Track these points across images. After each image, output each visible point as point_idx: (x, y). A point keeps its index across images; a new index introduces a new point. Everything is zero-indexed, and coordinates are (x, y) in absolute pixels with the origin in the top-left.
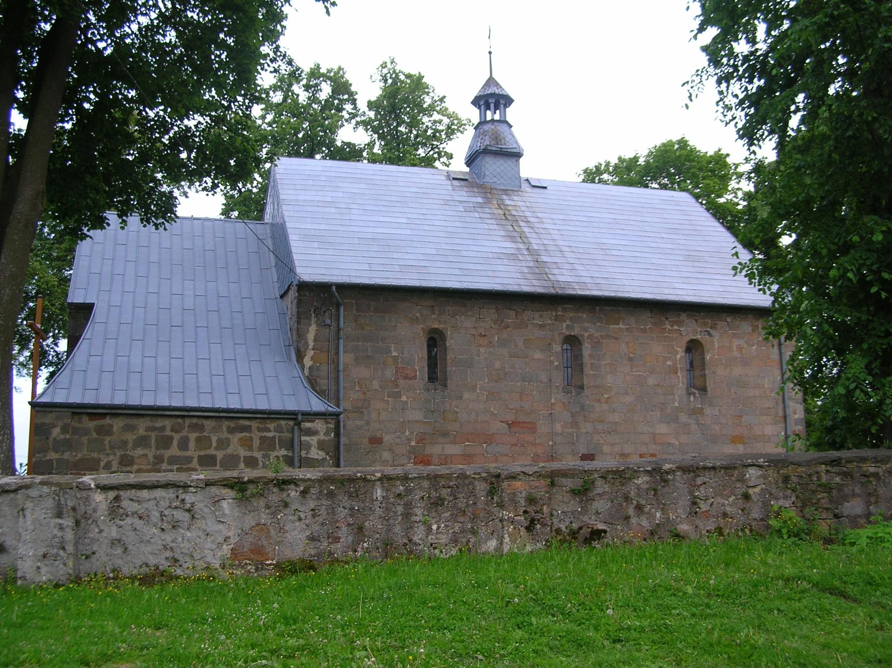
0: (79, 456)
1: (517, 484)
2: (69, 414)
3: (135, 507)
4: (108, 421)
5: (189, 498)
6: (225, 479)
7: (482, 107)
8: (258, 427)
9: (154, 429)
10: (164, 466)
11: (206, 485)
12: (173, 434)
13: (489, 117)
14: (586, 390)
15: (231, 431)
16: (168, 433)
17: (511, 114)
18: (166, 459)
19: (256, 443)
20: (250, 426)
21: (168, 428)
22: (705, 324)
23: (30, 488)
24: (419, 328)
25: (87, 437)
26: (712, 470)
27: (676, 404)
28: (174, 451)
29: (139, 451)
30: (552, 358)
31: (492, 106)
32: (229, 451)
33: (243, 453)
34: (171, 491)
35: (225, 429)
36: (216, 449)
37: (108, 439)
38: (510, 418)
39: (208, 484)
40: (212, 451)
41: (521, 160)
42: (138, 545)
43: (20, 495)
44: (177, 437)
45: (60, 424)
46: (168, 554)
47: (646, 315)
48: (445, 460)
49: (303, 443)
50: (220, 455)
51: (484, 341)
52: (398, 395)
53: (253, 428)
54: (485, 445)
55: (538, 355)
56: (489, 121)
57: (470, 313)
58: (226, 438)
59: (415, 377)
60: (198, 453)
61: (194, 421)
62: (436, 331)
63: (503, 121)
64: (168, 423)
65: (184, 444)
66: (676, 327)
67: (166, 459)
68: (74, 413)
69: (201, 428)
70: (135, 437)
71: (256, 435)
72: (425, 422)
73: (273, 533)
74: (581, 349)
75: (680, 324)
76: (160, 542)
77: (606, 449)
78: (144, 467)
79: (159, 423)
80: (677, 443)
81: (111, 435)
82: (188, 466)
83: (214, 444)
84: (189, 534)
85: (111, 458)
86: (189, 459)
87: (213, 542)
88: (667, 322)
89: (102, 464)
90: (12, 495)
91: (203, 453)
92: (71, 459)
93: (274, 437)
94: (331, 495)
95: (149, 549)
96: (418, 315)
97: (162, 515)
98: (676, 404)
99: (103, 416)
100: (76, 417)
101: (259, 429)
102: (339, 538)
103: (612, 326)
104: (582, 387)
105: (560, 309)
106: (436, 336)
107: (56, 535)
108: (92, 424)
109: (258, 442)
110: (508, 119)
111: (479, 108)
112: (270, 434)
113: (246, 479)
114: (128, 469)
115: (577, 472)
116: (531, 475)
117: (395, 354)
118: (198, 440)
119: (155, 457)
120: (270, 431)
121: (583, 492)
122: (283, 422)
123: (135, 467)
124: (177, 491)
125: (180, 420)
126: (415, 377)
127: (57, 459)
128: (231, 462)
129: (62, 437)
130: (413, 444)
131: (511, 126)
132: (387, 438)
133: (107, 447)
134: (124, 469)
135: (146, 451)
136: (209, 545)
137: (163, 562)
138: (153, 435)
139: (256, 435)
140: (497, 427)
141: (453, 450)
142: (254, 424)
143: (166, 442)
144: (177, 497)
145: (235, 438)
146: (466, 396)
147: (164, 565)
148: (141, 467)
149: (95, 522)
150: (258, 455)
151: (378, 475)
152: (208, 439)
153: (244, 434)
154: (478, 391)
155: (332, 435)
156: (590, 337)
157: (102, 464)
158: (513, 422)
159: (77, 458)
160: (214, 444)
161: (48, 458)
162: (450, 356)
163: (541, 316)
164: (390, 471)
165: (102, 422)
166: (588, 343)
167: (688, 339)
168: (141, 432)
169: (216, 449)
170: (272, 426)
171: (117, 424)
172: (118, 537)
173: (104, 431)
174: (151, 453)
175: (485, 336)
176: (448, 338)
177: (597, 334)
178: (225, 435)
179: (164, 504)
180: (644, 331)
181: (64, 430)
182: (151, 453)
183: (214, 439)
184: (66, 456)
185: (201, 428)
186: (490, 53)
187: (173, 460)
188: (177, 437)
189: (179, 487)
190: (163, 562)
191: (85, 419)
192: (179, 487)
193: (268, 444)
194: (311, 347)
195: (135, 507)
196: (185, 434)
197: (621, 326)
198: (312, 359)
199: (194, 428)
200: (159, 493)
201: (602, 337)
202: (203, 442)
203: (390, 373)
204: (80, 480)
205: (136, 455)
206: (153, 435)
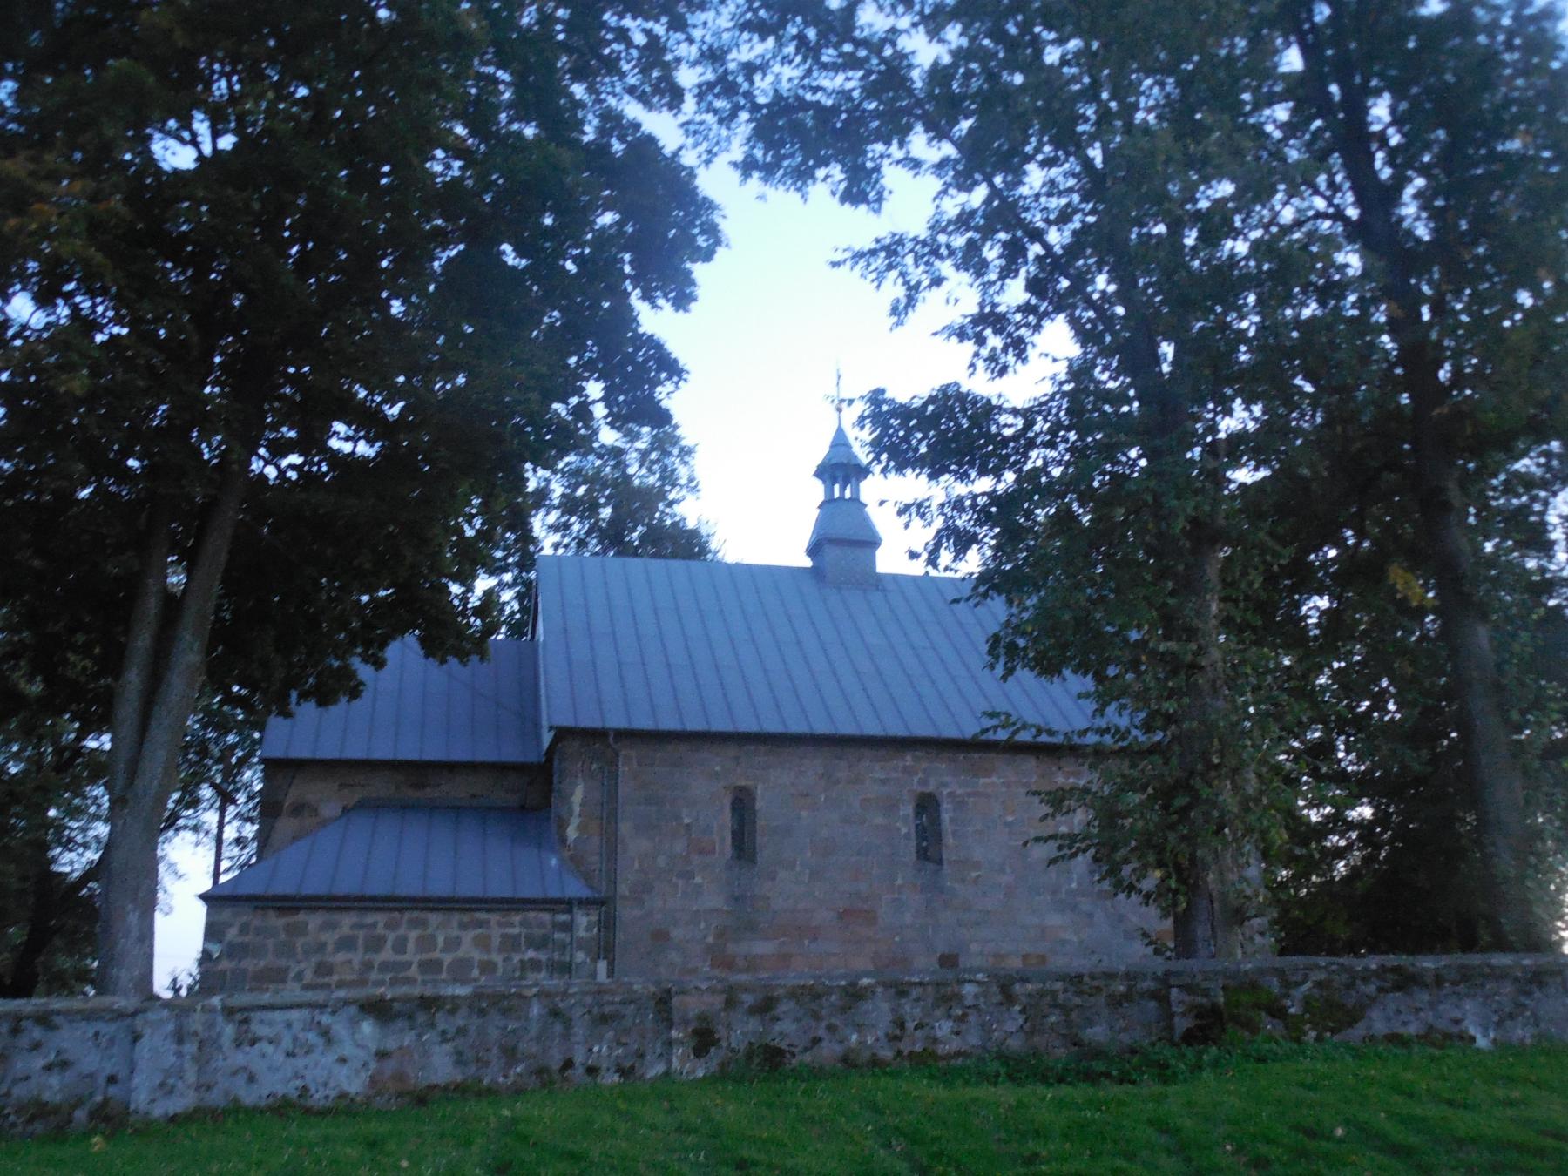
0: (262, 963)
1: (688, 999)
4: (301, 917)
12: (387, 932)
13: (837, 494)
14: (945, 866)
15: (463, 926)
16: (380, 930)
18: (376, 966)
20: (488, 922)
21: (381, 925)
28: (387, 955)
29: (340, 957)
31: (840, 479)
32: (461, 953)
33: (477, 955)
36: (442, 951)
37: (300, 942)
40: (436, 955)
46: (299, 1083)
48: (752, 964)
50: (447, 959)
52: (688, 876)
53: (492, 923)
59: (713, 851)
60: (418, 957)
61: (416, 914)
62: (741, 789)
63: (855, 499)
64: (380, 918)
65: (400, 946)
67: (376, 966)
69: (423, 924)
77: (974, 947)
79: (370, 918)
80: (1075, 939)
85: (303, 966)
86: (408, 965)
88: (1060, 773)
89: (292, 974)
91: (426, 956)
93: (520, 935)
94: (482, 1013)
98: (1074, 885)
101: (500, 924)
103: (982, 780)
104: (940, 862)
105: (909, 758)
112: (516, 931)
117: (687, 821)
118: (420, 940)
121: (765, 1007)
122: (532, 915)
123: (335, 978)
125: (396, 915)
126: (713, 851)
129: (240, 940)
132: (677, 933)
135: (350, 956)
138: (361, 934)
141: (762, 948)
142: (494, 918)
143: (376, 944)
145: (468, 936)
146: (782, 874)
147: (294, 1095)
149: (220, 1048)
150: (497, 958)
152: (433, 937)
153: (480, 931)
154: (798, 869)
155: (596, 930)
157: (292, 974)
161: (219, 968)
162: (760, 823)
169: (442, 951)
170: (517, 918)
171: (314, 921)
173: (295, 931)
174: (357, 958)
176: (759, 798)
177: (959, 791)
178: (455, 932)
179: (297, 1026)
181: (244, 930)
182: (357, 958)
183: (440, 940)
185: (423, 924)
187: (385, 967)
188: (391, 937)
191: (271, 913)
198: (579, 828)
199: (414, 924)
201: (969, 795)
202: (426, 943)
203: (680, 847)
206: (361, 934)
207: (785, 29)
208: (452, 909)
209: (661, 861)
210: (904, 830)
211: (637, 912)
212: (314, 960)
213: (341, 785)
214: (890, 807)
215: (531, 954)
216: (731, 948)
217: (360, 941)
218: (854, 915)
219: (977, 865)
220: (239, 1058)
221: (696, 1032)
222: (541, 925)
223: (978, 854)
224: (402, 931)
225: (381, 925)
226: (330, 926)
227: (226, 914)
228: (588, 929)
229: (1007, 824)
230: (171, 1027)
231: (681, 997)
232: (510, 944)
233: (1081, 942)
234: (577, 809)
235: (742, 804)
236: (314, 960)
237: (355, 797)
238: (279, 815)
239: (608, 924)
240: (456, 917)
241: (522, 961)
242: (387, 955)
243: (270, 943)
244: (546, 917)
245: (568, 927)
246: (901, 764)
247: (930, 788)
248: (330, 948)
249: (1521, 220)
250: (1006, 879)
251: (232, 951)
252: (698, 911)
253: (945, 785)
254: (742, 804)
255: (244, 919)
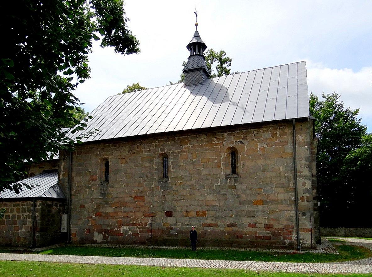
15: (14, 206)
32: (13, 213)
33: (17, 214)
40: (9, 214)
50: (11, 215)
52: (90, 187)
59: (97, 180)
80: (218, 205)
112: (24, 207)
117: (90, 170)
126: (97, 180)
141: (109, 210)
150: (21, 215)
170: (25, 203)
177: (176, 151)
203: (88, 178)
209: (83, 184)
215: (28, 213)
216: (101, 210)
218: (139, 198)
219: (181, 178)
223: (181, 174)
229: (194, 162)
232: (24, 211)
233: (220, 206)
234: (62, 169)
237: (42, 170)
246: (154, 144)
249: (74, 16)
250: (193, 182)
252: (92, 198)
253: (170, 150)
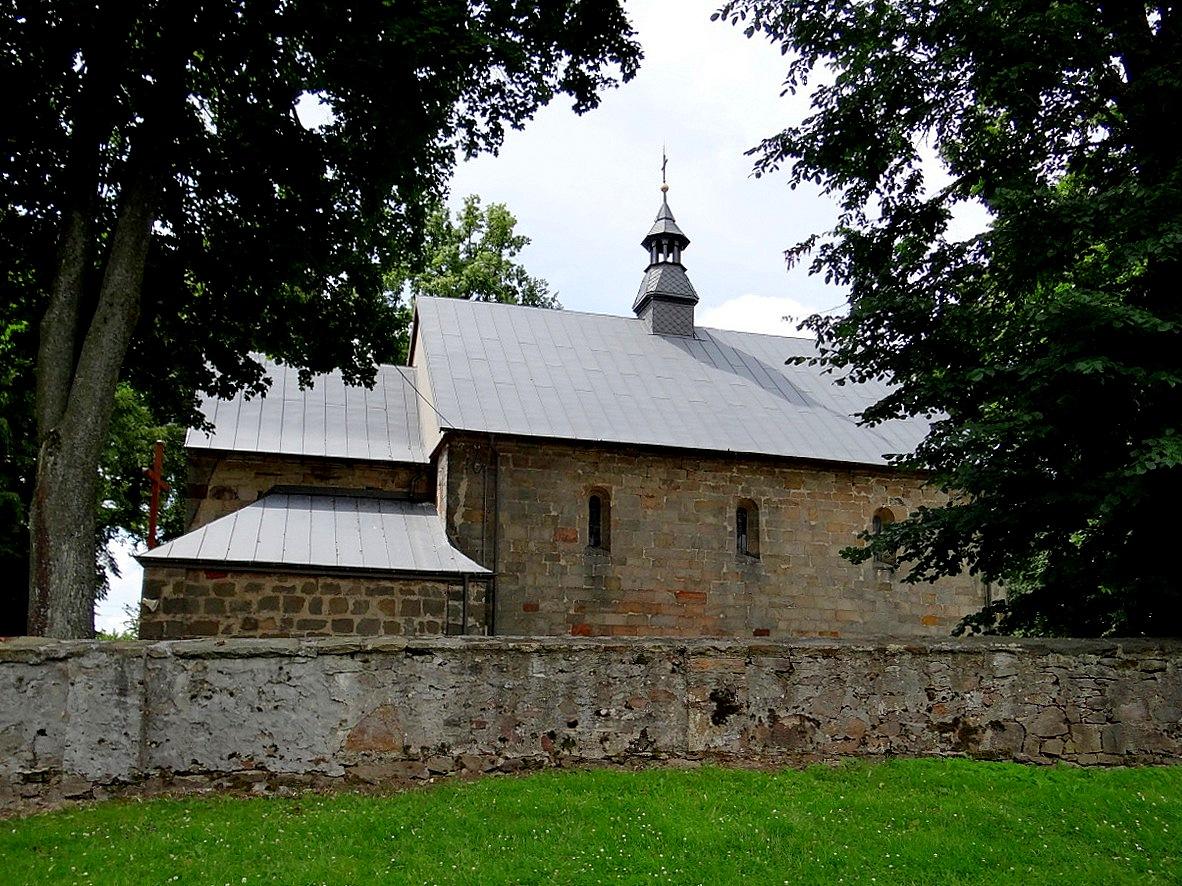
1: (709, 662)
2: (184, 571)
3: (226, 682)
4: (229, 579)
5: (296, 670)
6: (343, 647)
7: (654, 249)
8: (401, 589)
9: (283, 589)
10: (294, 631)
11: (318, 654)
12: (304, 595)
15: (370, 593)
16: (298, 593)
17: (686, 257)
18: (295, 624)
19: (398, 607)
21: (299, 589)
22: (896, 491)
23: (83, 656)
24: (580, 486)
25: (204, 598)
26: (949, 655)
27: (861, 578)
28: (305, 614)
29: (265, 614)
30: (725, 524)
32: (368, 615)
34: (273, 661)
35: (363, 591)
36: (352, 613)
37: (228, 600)
38: (678, 587)
39: (322, 653)
40: (348, 616)
41: (696, 308)
42: (226, 730)
43: (71, 664)
44: (308, 598)
45: (172, 581)
46: (268, 742)
47: (831, 478)
49: (450, 608)
50: (357, 620)
51: (650, 502)
52: (557, 558)
54: (650, 616)
55: (711, 520)
56: (662, 263)
57: (637, 472)
58: (365, 601)
59: (575, 540)
61: (329, 580)
63: (677, 264)
64: (298, 583)
65: (316, 608)
66: (863, 494)
67: (295, 624)
68: (188, 570)
69: (337, 589)
70: (260, 598)
71: (398, 598)
72: (586, 589)
73: (401, 717)
74: (757, 515)
75: (868, 490)
76: (256, 726)
77: (782, 625)
78: (270, 633)
80: (861, 621)
81: (232, 595)
82: (321, 631)
83: (351, 607)
84: (294, 717)
85: (231, 621)
86: (323, 624)
87: (324, 727)
89: (221, 628)
90: (60, 664)
91: (338, 617)
92: (185, 622)
93: (418, 602)
95: (242, 734)
96: (580, 472)
97: (261, 692)
98: (861, 578)
99: (224, 573)
100: (191, 574)
102: (486, 723)
104: (757, 556)
106: (599, 495)
107: (116, 717)
108: (210, 583)
109: (401, 606)
110: (682, 263)
111: (651, 251)
113: (369, 648)
114: (251, 633)
115: (781, 650)
116: (725, 652)
118: (332, 602)
119: (284, 621)
120: (414, 594)
122: (429, 584)
123: (260, 632)
124: (281, 662)
125: (312, 580)
126: (575, 540)
127: (167, 622)
128: (369, 627)
130: (572, 612)
131: (685, 270)
133: (228, 609)
134: (247, 634)
136: (319, 731)
137: (260, 751)
139: (398, 598)
140: (663, 596)
141: (611, 619)
142: (397, 586)
143: (295, 604)
144: (281, 668)
145: (375, 601)
146: (630, 562)
148: (266, 631)
151: (535, 645)
153: (386, 597)
156: (767, 501)
158: (682, 592)
159: (192, 621)
160: (351, 607)
162: (614, 517)
163: (714, 477)
164: (549, 641)
165: (221, 581)
166: (765, 508)
167: (877, 507)
168: (268, 592)
170: (416, 588)
171: (240, 583)
172: (201, 720)
174: (278, 616)
175: (652, 497)
178: (364, 598)
179: (262, 678)
180: (828, 496)
181: (177, 587)
182: (278, 616)
184: (179, 617)
185: (337, 589)
186: (665, 190)
187: (303, 624)
189: (284, 656)
190: (260, 751)
191: (202, 575)
192: (284, 656)
193: (411, 609)
194: (462, 504)
195: (226, 682)
196: (318, 595)
197: (802, 490)
199: (328, 588)
200: (258, 664)
203: (547, 534)
204: (153, 646)
205: (261, 619)
207: (125, 634)
208: (359, 578)
210: (730, 529)
211: (513, 587)
212: (241, 616)
213: (257, 473)
214: (720, 511)
215: (429, 618)
216: (588, 619)
217: (281, 602)
219: (787, 560)
220: (196, 713)
221: (714, 697)
222: (438, 593)
223: (788, 549)
224: (318, 594)
225: (299, 589)
226: (256, 588)
227: (161, 575)
228: (477, 599)
229: (812, 527)
230: (110, 674)
231: (700, 659)
235: (598, 505)
236: (241, 616)
237: (271, 483)
238: (205, 497)
239: (491, 595)
240: (365, 584)
241: (421, 623)
242: (305, 614)
243: (202, 600)
244: (442, 587)
245: (462, 596)
246: (729, 474)
247: (752, 495)
248: (255, 607)
250: (810, 571)
251: (168, 606)
254: (598, 505)
255: (179, 578)
